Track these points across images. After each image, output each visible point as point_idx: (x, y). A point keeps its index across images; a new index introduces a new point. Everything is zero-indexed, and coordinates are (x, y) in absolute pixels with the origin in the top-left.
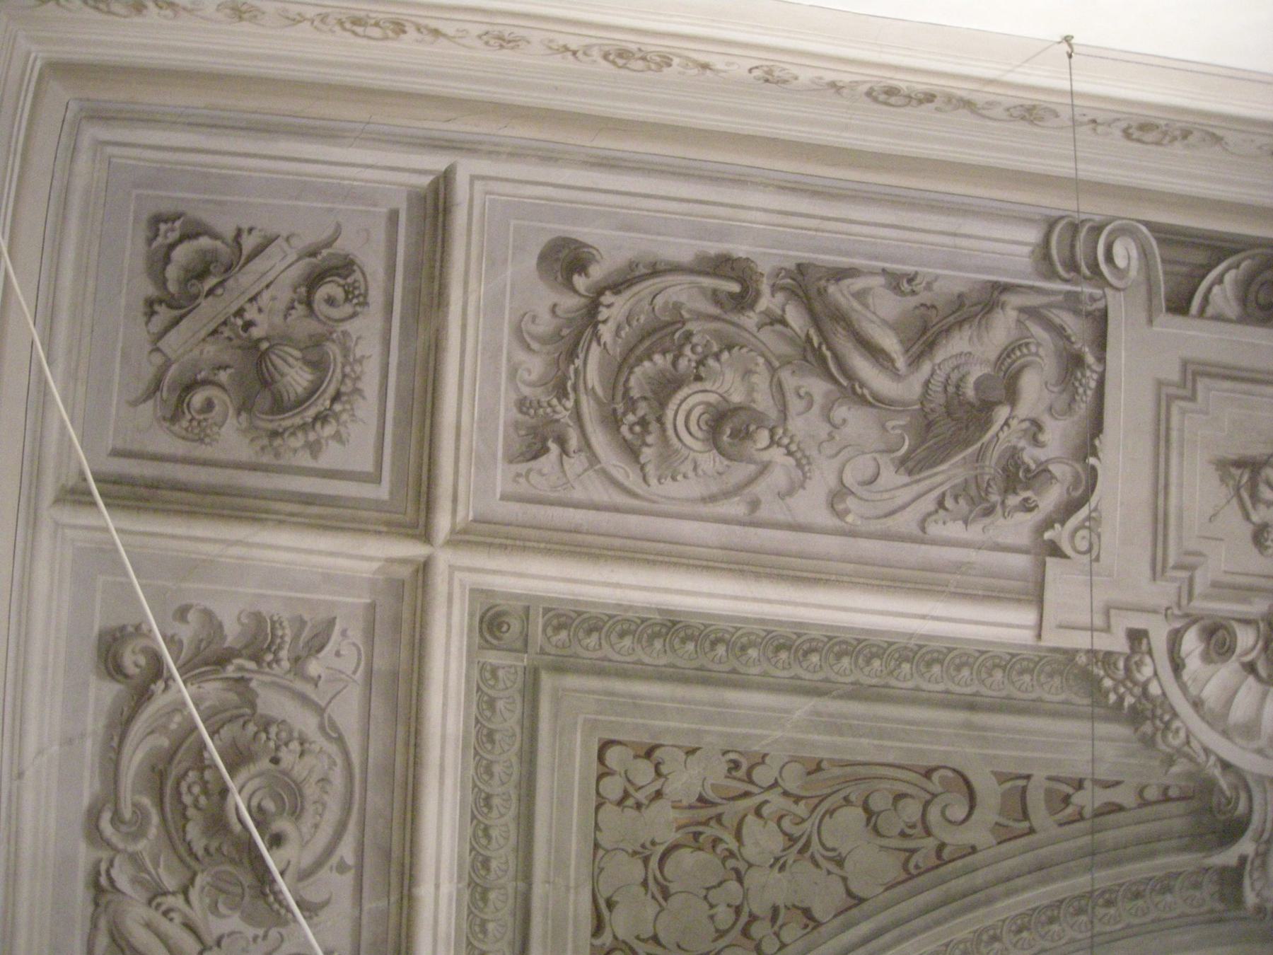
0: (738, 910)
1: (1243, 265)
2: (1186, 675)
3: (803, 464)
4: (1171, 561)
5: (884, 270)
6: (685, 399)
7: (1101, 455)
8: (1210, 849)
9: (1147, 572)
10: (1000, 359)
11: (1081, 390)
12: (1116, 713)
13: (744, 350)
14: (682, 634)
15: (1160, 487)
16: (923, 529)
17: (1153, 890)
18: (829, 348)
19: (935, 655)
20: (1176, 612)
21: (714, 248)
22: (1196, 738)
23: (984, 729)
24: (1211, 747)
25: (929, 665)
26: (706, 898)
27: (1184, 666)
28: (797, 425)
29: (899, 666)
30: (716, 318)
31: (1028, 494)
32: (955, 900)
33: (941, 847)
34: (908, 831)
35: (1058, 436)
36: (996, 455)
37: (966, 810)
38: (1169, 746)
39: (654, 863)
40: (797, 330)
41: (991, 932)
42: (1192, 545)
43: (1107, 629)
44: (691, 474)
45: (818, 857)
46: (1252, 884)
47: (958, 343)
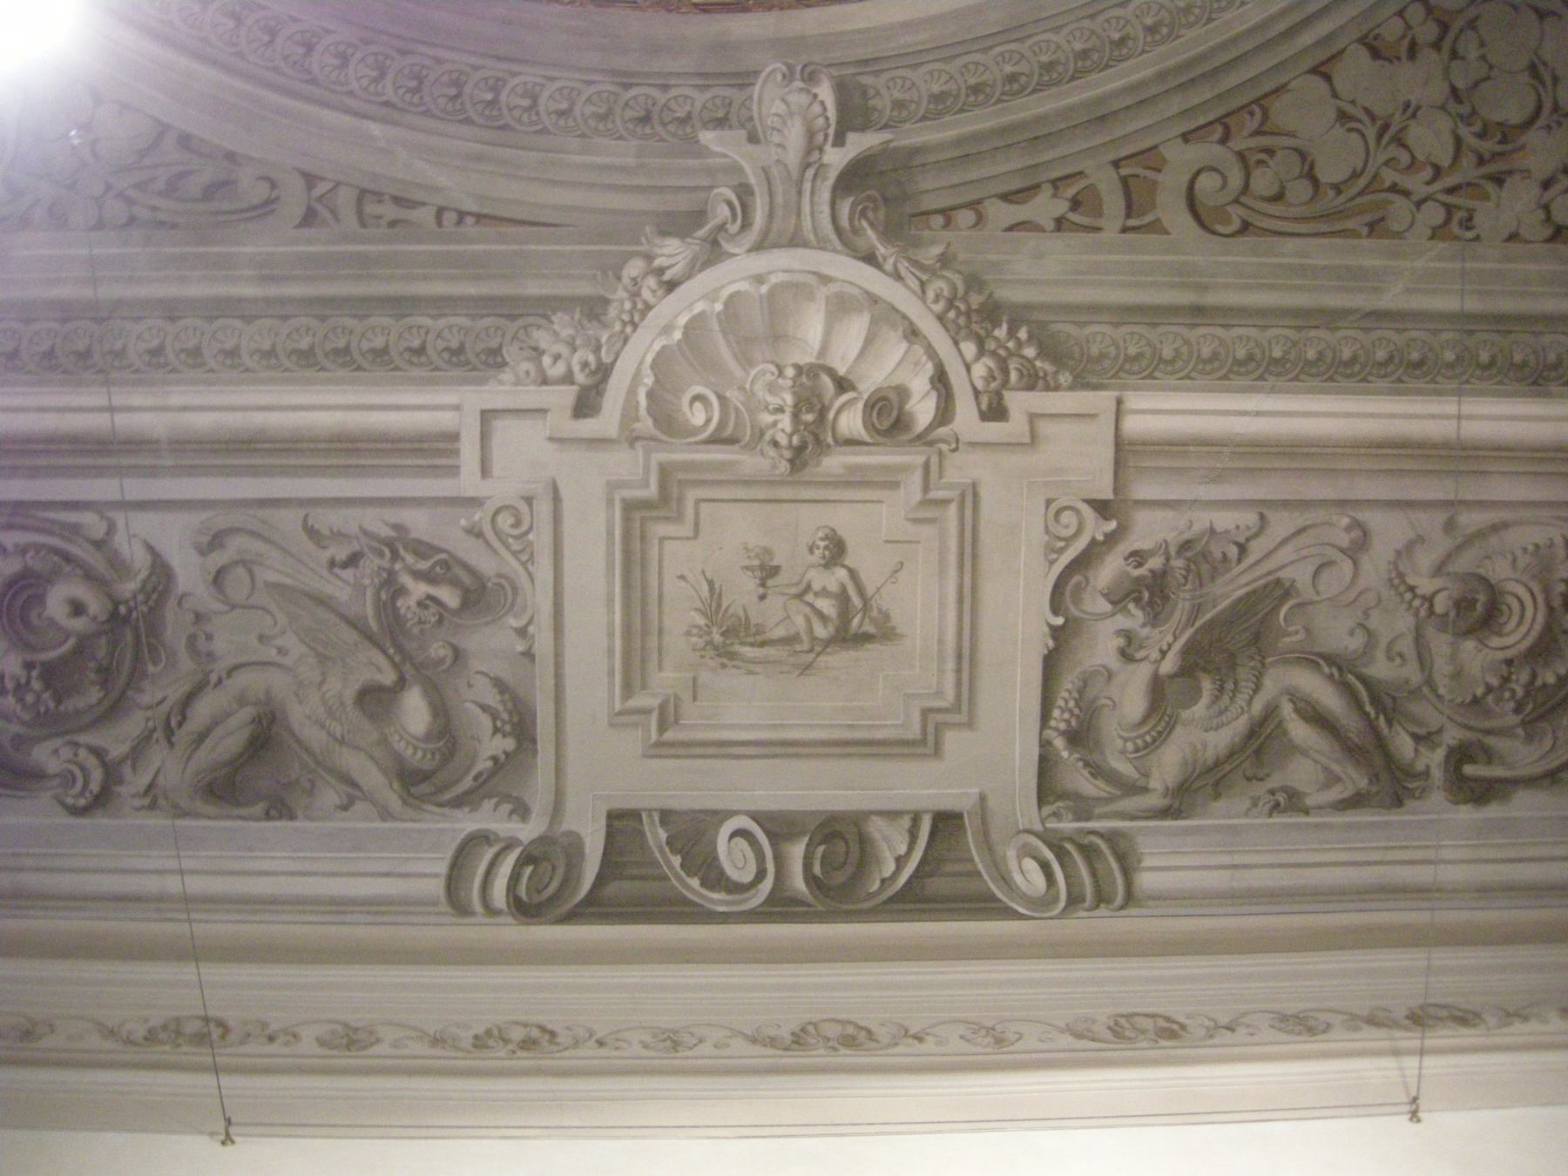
0: (1454, 55)
1: (876, 886)
2: (929, 368)
3: (1399, 582)
4: (953, 508)
5: (1307, 813)
6: (1523, 638)
7: (1046, 629)
8: (886, 152)
9: (984, 492)
10: (1170, 728)
11: (1071, 704)
12: (1018, 316)
13: (1459, 700)
14: (1527, 370)
15: (969, 600)
16: (1262, 517)
17: (957, 97)
18: (1367, 714)
19: (1243, 370)
20: (944, 447)
21: (1493, 811)
22: (914, 292)
23: (1183, 285)
24: (890, 281)
25: (1250, 357)
26: (1491, 67)
27: (932, 381)
28: (1404, 623)
29: (1286, 353)
30: (1489, 732)
31: (1137, 573)
32: (1204, 75)
33: (1223, 141)
34: (1263, 156)
35: (1101, 647)
36: (1177, 614)
37: (1197, 186)
38: (948, 280)
39: (1547, 106)
40: (1400, 729)
41: (1158, 37)
42: (927, 532)
43: (1033, 418)
44: (1519, 553)
45: (1365, 119)
46: (825, 109)
47: (1220, 740)
